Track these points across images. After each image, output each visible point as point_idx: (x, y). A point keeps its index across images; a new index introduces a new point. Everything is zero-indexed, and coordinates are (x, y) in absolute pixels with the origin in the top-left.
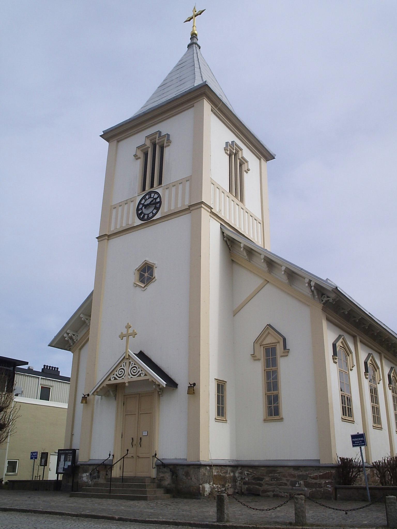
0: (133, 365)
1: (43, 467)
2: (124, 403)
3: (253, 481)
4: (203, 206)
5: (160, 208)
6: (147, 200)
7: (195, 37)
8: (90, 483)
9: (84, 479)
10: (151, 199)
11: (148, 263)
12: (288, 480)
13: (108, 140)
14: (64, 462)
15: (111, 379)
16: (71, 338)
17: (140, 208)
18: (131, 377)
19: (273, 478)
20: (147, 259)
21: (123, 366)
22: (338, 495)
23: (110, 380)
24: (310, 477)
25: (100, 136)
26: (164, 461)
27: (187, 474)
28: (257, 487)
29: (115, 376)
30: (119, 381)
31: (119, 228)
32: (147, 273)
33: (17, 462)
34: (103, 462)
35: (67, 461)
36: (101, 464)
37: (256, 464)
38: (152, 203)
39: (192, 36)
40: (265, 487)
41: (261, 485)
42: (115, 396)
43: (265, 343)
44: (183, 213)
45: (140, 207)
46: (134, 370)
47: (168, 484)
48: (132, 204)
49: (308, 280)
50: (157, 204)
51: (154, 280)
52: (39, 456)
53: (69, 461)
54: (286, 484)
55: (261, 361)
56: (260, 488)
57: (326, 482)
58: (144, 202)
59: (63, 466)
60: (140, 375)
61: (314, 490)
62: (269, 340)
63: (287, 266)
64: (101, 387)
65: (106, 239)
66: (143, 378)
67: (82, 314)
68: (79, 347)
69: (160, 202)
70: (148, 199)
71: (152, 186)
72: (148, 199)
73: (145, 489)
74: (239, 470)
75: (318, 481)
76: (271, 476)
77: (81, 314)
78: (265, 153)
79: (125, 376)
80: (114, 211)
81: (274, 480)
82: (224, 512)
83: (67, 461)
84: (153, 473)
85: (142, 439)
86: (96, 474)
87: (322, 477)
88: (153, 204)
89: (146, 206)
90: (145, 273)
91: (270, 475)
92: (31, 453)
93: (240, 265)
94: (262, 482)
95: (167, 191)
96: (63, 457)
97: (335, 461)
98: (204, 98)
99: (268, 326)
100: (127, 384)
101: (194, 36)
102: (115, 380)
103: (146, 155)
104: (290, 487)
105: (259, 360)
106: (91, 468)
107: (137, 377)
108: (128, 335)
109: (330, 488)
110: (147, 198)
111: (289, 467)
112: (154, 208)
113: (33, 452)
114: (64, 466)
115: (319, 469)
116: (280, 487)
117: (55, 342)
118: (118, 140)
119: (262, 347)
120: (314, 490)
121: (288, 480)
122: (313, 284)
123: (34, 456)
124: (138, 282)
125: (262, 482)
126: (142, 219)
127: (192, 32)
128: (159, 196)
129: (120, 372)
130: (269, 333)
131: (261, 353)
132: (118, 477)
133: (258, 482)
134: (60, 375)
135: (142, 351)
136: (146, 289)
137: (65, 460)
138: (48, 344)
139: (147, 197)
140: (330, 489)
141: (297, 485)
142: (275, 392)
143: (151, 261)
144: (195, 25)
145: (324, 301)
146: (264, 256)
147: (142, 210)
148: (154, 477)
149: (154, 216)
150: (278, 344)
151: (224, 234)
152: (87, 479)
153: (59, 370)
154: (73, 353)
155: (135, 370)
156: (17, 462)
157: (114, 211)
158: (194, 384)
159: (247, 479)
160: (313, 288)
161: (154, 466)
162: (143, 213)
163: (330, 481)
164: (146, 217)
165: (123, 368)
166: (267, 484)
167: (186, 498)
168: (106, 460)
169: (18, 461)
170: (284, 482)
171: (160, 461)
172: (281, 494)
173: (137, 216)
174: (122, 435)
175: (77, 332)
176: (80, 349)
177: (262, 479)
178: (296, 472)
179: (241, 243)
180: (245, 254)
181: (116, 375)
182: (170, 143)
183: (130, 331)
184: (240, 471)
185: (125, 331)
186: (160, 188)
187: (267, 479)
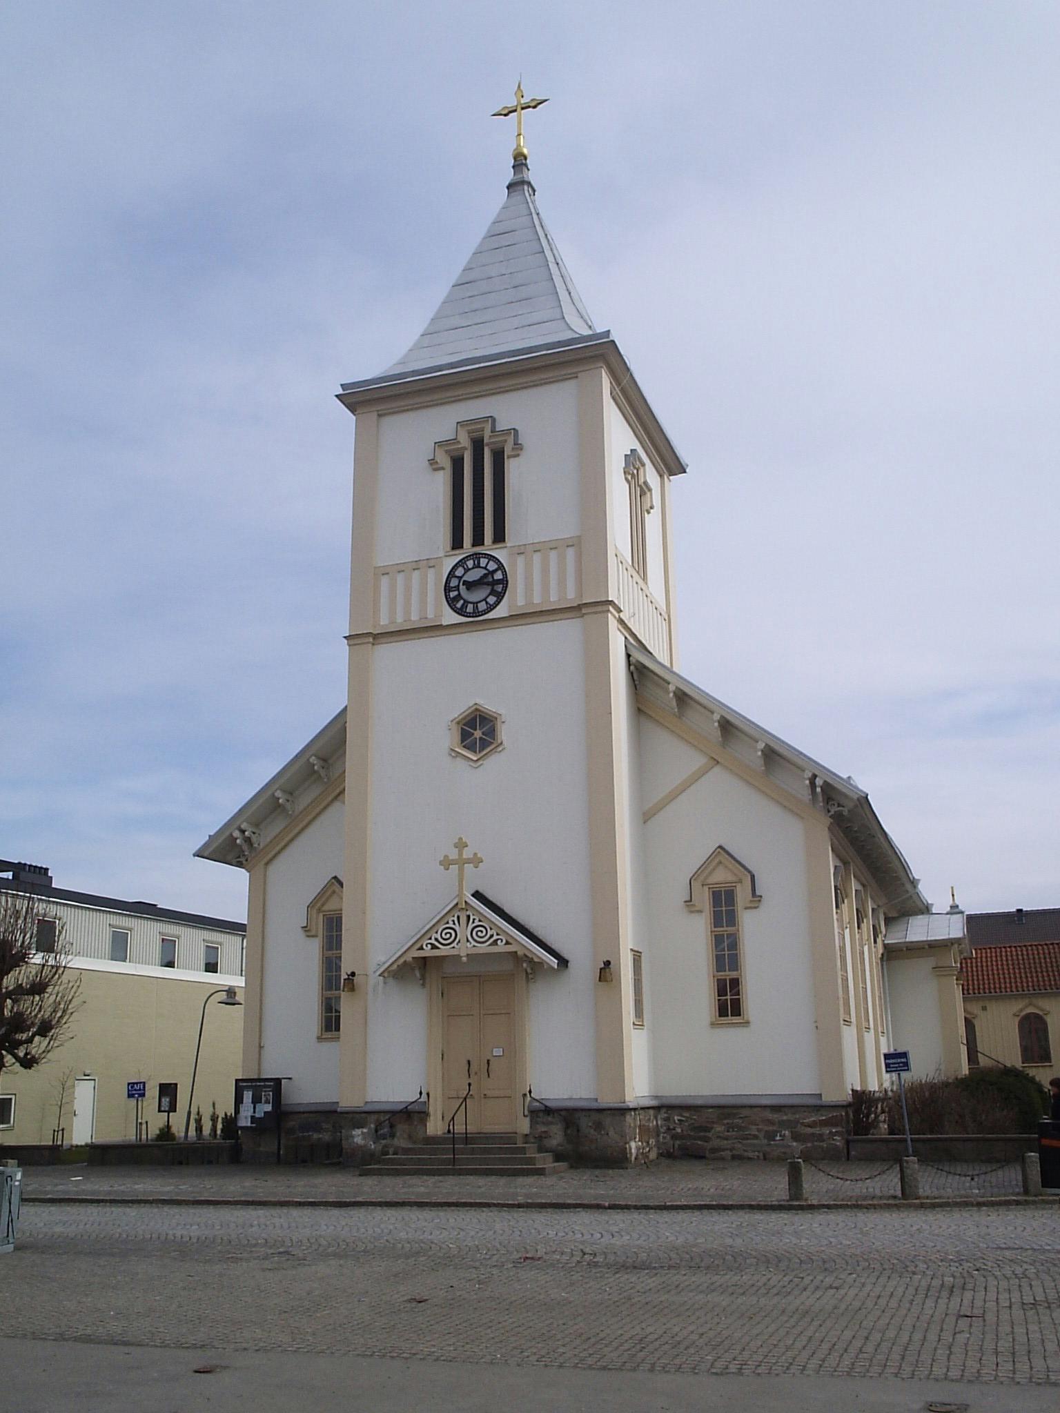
0: (477, 923)
1: (166, 1114)
2: (442, 994)
3: (692, 1134)
4: (611, 608)
5: (505, 593)
6: (470, 569)
7: (522, 164)
8: (373, 1147)
9: (355, 1140)
10: (481, 572)
11: (481, 708)
12: (759, 1130)
13: (352, 408)
14: (252, 1106)
15: (424, 947)
16: (248, 840)
17: (452, 585)
18: (474, 946)
19: (730, 1128)
20: (480, 701)
21: (451, 922)
22: (853, 1153)
23: (421, 948)
24: (802, 1124)
25: (337, 396)
26: (548, 1104)
27: (598, 1126)
28: (699, 1142)
29: (433, 941)
30: (444, 951)
31: (400, 622)
32: (478, 731)
33: (11, 1099)
34: (406, 1107)
35: (261, 1102)
36: (401, 1111)
37: (699, 1102)
38: (485, 580)
39: (515, 159)
40: (716, 1143)
41: (707, 1140)
42: (423, 977)
43: (711, 880)
44: (560, 616)
45: (454, 583)
46: (479, 934)
47: (558, 1145)
48: (431, 574)
49: (810, 775)
50: (496, 585)
51: (500, 749)
52: (153, 1092)
53: (267, 1102)
54: (756, 1137)
55: (704, 914)
56: (706, 1144)
57: (831, 1132)
58: (463, 575)
59: (250, 1113)
60: (495, 942)
61: (809, 1145)
62: (721, 876)
63: (768, 743)
64: (402, 960)
65: (368, 643)
66: (501, 947)
67: (278, 791)
68: (266, 860)
69: (504, 582)
70: (473, 568)
71: (478, 540)
72: (473, 568)
73: (525, 1154)
74: (663, 1115)
75: (817, 1130)
76: (728, 1124)
77: (276, 790)
78: (668, 455)
79: (459, 942)
80: (385, 580)
81: (733, 1131)
82: (801, 1186)
83: (261, 1102)
84: (524, 1126)
85: (491, 1063)
86: (386, 1130)
87: (824, 1123)
88: (487, 584)
89: (470, 586)
90: (475, 730)
91: (726, 1122)
92: (129, 1084)
93: (657, 721)
94: (710, 1135)
95: (520, 561)
96: (248, 1096)
97: (847, 1097)
98: (602, 367)
99: (719, 850)
100: (464, 959)
101: (520, 162)
102: (432, 949)
103: (457, 463)
104: (766, 1141)
105: (700, 911)
106: (374, 1117)
107: (489, 945)
108: (461, 862)
109: (839, 1141)
110: (470, 566)
111: (765, 1107)
112: (488, 591)
113: (134, 1083)
114: (254, 1112)
115: (818, 1110)
116: (745, 1142)
117: (211, 849)
118: (380, 412)
119: (706, 888)
120: (809, 1145)
121: (759, 1130)
122: (819, 782)
123: (135, 1090)
124: (459, 748)
125: (710, 1135)
126: (461, 612)
127: (514, 150)
128: (501, 567)
129: (446, 934)
130: (720, 862)
131: (704, 899)
132: (439, 1133)
133: (702, 1134)
134: (53, 886)
135: (481, 891)
136: (481, 765)
137: (256, 1100)
138: (194, 852)
139: (470, 564)
140: (838, 1144)
141: (778, 1138)
142: (734, 974)
143: (490, 706)
144: (522, 132)
145: (832, 813)
146: (764, 745)
147: (458, 590)
148: (525, 1133)
149: (491, 610)
150: (739, 886)
151: (631, 658)
152: (364, 1139)
153: (50, 875)
154: (249, 872)
155: (482, 932)
156: (11, 1099)
157: (385, 580)
158: (607, 963)
159: (679, 1130)
160: (818, 790)
161: (526, 1113)
162: (462, 598)
163: (839, 1129)
164: (470, 608)
165: (453, 926)
166: (718, 1137)
167: (597, 1167)
168: (413, 1102)
169: (13, 1097)
170: (753, 1133)
171: (538, 1104)
172: (746, 1154)
173: (446, 603)
174: (443, 1055)
175: (257, 825)
176: (267, 864)
177: (707, 1130)
178: (775, 1116)
179: (669, 683)
180: (674, 703)
181: (436, 940)
182: (521, 449)
183: (467, 854)
184: (666, 1115)
185: (454, 854)
186: (502, 550)
187: (719, 1128)
